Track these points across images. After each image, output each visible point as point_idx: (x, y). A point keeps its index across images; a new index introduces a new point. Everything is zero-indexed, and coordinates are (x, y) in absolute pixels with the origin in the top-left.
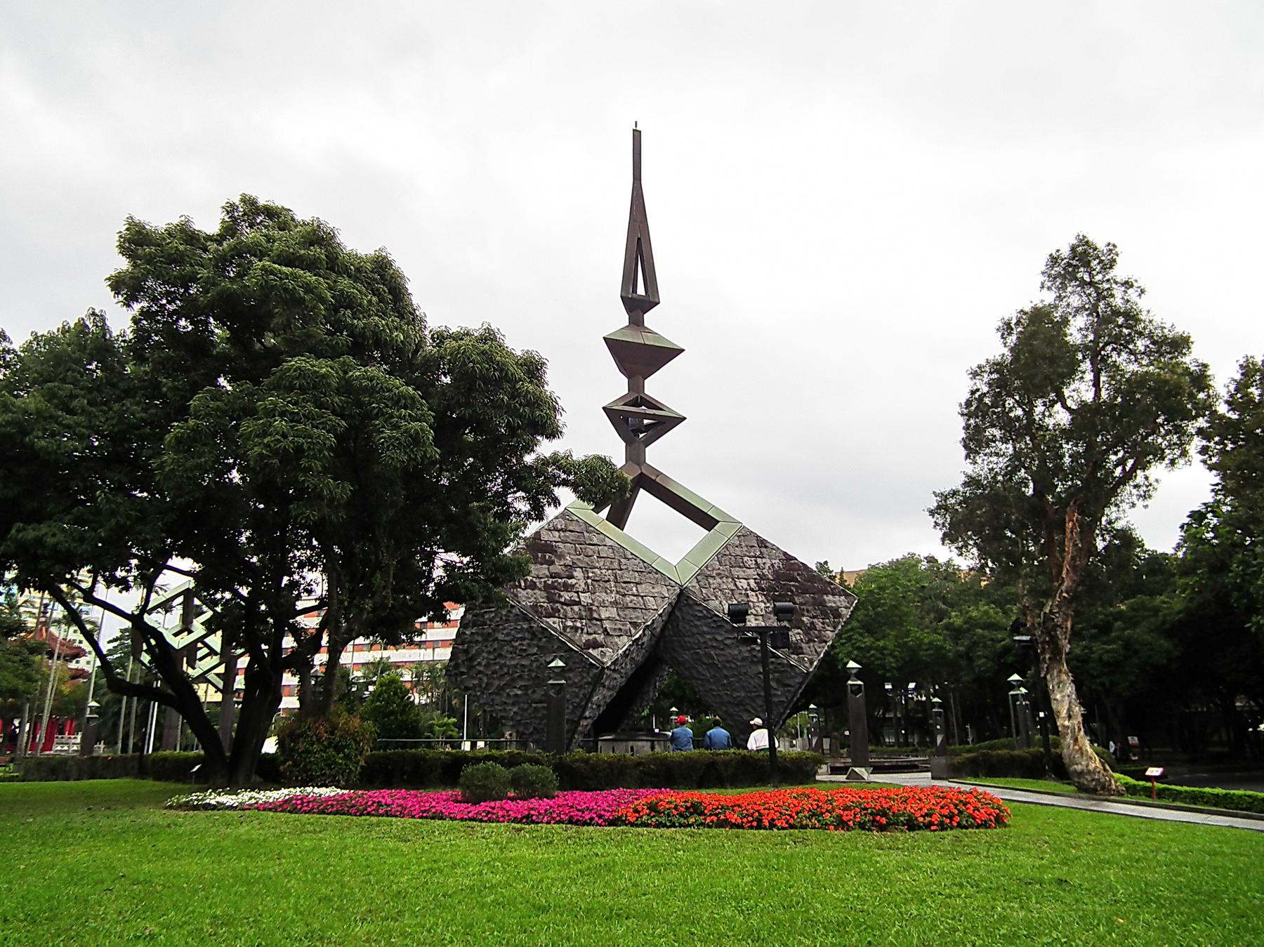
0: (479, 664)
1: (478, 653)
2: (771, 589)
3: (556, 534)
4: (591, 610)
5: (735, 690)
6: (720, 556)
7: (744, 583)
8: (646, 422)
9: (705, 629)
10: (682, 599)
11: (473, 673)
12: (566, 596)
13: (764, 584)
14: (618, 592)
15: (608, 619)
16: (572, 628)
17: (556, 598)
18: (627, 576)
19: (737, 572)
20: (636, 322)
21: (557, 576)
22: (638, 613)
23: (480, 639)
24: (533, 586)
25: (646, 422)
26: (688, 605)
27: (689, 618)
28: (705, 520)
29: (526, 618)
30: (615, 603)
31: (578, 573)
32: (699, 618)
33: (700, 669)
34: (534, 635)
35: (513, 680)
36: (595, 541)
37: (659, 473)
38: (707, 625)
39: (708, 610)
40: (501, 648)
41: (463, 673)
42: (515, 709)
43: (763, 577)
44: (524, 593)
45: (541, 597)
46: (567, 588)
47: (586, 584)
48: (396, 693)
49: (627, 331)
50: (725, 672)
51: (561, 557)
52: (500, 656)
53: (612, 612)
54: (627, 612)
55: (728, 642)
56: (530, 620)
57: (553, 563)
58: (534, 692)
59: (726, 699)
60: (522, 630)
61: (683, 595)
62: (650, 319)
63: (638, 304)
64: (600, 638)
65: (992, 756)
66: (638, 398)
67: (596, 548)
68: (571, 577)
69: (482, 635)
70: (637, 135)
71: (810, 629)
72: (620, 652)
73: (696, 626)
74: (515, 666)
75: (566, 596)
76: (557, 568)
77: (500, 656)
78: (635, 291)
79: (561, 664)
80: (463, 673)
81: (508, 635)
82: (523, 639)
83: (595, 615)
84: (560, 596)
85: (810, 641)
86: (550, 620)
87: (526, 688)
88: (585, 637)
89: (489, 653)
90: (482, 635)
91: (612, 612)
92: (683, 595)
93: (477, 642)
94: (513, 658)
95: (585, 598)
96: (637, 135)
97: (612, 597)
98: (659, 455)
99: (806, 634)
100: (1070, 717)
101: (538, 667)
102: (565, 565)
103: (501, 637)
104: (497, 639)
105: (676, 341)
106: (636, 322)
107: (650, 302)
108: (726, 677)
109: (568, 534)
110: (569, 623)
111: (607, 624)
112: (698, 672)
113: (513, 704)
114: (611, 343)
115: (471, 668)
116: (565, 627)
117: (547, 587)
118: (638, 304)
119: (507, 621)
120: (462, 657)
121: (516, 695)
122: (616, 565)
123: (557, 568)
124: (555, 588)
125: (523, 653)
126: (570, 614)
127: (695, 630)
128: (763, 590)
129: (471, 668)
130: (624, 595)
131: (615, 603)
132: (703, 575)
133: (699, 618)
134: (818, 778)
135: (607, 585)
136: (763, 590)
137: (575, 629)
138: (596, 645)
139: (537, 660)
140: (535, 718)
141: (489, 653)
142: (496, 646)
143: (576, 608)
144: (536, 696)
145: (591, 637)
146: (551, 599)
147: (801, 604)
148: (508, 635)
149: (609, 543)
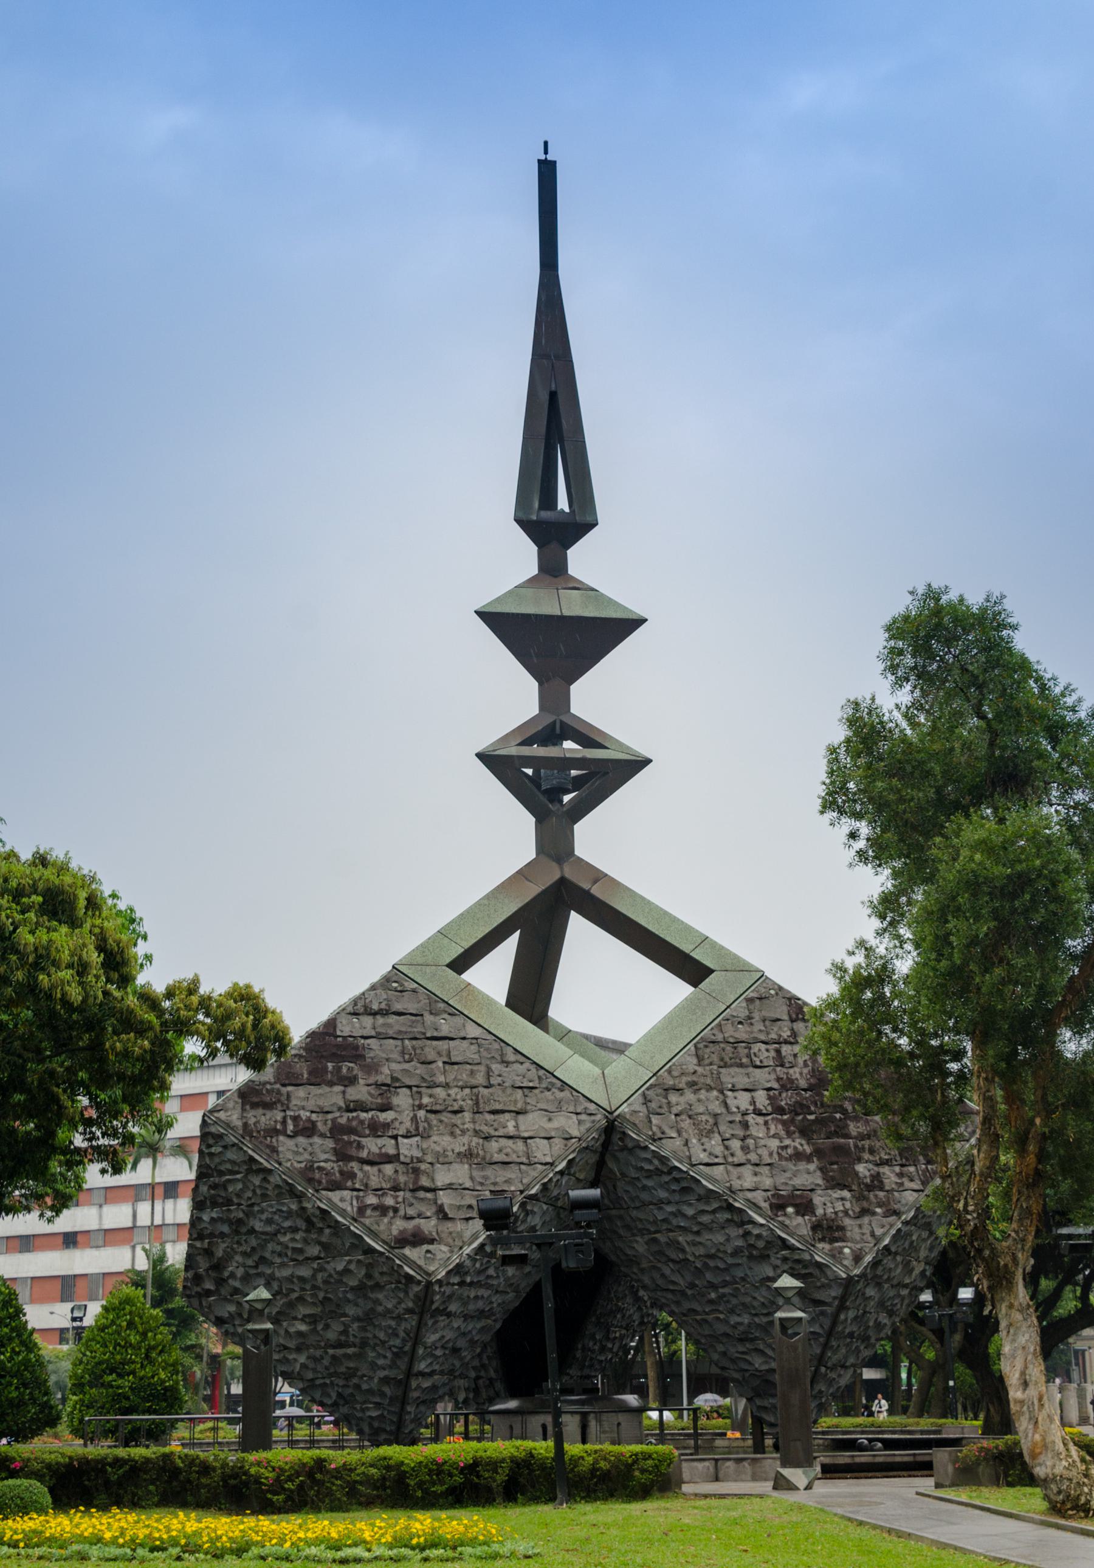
0: (232, 1275)
1: (228, 1257)
2: (799, 1108)
3: (368, 1021)
4: (416, 1171)
5: (732, 1311)
6: (702, 1046)
7: (742, 1101)
8: (574, 773)
9: (663, 1194)
10: (615, 1138)
11: (224, 1291)
12: (372, 1145)
13: (786, 1100)
14: (477, 1133)
15: (450, 1187)
16: (375, 1208)
17: (353, 1152)
18: (501, 1099)
19: (732, 1076)
20: (552, 568)
21: (361, 1107)
22: (511, 1173)
23: (225, 1229)
24: (308, 1130)
25: (574, 773)
26: (624, 1148)
27: (633, 1174)
28: (689, 968)
29: (292, 1192)
30: (468, 1156)
31: (402, 1099)
32: (649, 1174)
33: (667, 1272)
34: (309, 1221)
35: (291, 1305)
36: (445, 1031)
37: (598, 876)
38: (664, 1186)
39: (663, 1160)
40: (262, 1247)
41: (208, 1293)
42: (302, 1359)
43: (787, 1084)
44: (291, 1143)
45: (321, 1149)
46: (377, 1129)
47: (414, 1119)
48: (131, 1325)
49: (529, 592)
50: (709, 1276)
51: (372, 1068)
52: (263, 1260)
53: (460, 1173)
54: (489, 1172)
55: (705, 1219)
56: (299, 1197)
57: (351, 1081)
58: (327, 1327)
59: (721, 1328)
60: (290, 1214)
61: (612, 1130)
62: (581, 559)
63: (554, 518)
64: (429, 1226)
65: (622, 1454)
66: (555, 725)
67: (443, 1045)
68: (385, 1108)
69: (230, 1222)
70: (547, 171)
71: (870, 1188)
72: (467, 1250)
73: (645, 1188)
74: (290, 1279)
75: (372, 1145)
76: (360, 1092)
77: (263, 1260)
78: (549, 499)
79: (265, 1294)
80: (208, 1293)
81: (269, 1222)
82: (294, 1230)
83: (424, 1182)
84: (360, 1146)
85: (864, 1212)
86: (335, 1196)
87: (312, 1320)
88: (399, 1225)
89: (245, 1254)
90: (230, 1222)
91: (460, 1173)
92: (612, 1130)
93: (222, 1235)
94: (283, 1265)
95: (408, 1148)
96: (547, 171)
97: (460, 1145)
98: (598, 838)
99: (860, 1198)
100: (1025, 1384)
101: (326, 1282)
102: (378, 1085)
103: (258, 1226)
104: (252, 1231)
105: (632, 603)
106: (552, 568)
107: (579, 525)
108: (713, 1286)
109: (392, 1019)
110: (372, 1200)
111: (444, 1198)
112: (663, 1275)
113: (298, 1350)
114: (500, 622)
115: (220, 1282)
116: (362, 1210)
117: (337, 1130)
118: (554, 518)
119: (264, 1196)
120: (203, 1264)
121: (300, 1334)
122: (480, 1079)
123: (360, 1092)
124: (352, 1131)
125: (298, 1257)
126: (374, 1182)
127: (645, 1196)
128: (780, 1110)
129: (220, 1282)
130: (487, 1138)
131: (468, 1156)
132: (660, 1088)
133: (649, 1174)
134: (685, 1488)
135: (457, 1119)
136: (780, 1110)
137: (383, 1210)
138: (417, 1239)
139: (322, 1269)
140: (336, 1374)
141: (245, 1254)
142: (254, 1242)
143: (388, 1169)
144: (331, 1335)
145: (410, 1225)
146: (342, 1155)
147: (862, 1137)
148: (269, 1222)
149: (473, 1031)
